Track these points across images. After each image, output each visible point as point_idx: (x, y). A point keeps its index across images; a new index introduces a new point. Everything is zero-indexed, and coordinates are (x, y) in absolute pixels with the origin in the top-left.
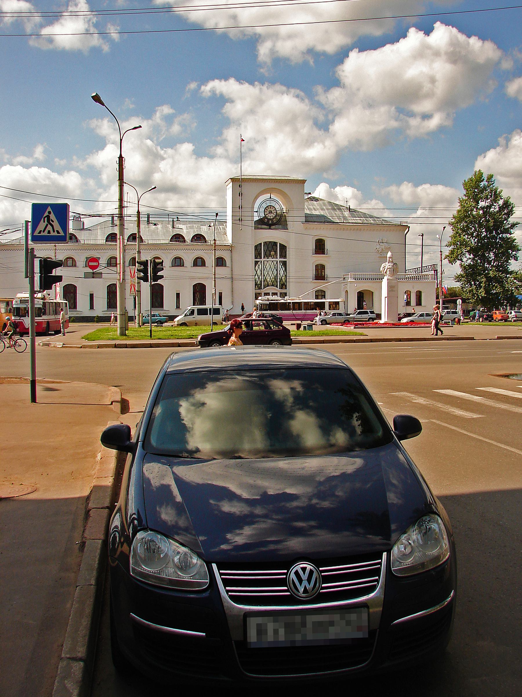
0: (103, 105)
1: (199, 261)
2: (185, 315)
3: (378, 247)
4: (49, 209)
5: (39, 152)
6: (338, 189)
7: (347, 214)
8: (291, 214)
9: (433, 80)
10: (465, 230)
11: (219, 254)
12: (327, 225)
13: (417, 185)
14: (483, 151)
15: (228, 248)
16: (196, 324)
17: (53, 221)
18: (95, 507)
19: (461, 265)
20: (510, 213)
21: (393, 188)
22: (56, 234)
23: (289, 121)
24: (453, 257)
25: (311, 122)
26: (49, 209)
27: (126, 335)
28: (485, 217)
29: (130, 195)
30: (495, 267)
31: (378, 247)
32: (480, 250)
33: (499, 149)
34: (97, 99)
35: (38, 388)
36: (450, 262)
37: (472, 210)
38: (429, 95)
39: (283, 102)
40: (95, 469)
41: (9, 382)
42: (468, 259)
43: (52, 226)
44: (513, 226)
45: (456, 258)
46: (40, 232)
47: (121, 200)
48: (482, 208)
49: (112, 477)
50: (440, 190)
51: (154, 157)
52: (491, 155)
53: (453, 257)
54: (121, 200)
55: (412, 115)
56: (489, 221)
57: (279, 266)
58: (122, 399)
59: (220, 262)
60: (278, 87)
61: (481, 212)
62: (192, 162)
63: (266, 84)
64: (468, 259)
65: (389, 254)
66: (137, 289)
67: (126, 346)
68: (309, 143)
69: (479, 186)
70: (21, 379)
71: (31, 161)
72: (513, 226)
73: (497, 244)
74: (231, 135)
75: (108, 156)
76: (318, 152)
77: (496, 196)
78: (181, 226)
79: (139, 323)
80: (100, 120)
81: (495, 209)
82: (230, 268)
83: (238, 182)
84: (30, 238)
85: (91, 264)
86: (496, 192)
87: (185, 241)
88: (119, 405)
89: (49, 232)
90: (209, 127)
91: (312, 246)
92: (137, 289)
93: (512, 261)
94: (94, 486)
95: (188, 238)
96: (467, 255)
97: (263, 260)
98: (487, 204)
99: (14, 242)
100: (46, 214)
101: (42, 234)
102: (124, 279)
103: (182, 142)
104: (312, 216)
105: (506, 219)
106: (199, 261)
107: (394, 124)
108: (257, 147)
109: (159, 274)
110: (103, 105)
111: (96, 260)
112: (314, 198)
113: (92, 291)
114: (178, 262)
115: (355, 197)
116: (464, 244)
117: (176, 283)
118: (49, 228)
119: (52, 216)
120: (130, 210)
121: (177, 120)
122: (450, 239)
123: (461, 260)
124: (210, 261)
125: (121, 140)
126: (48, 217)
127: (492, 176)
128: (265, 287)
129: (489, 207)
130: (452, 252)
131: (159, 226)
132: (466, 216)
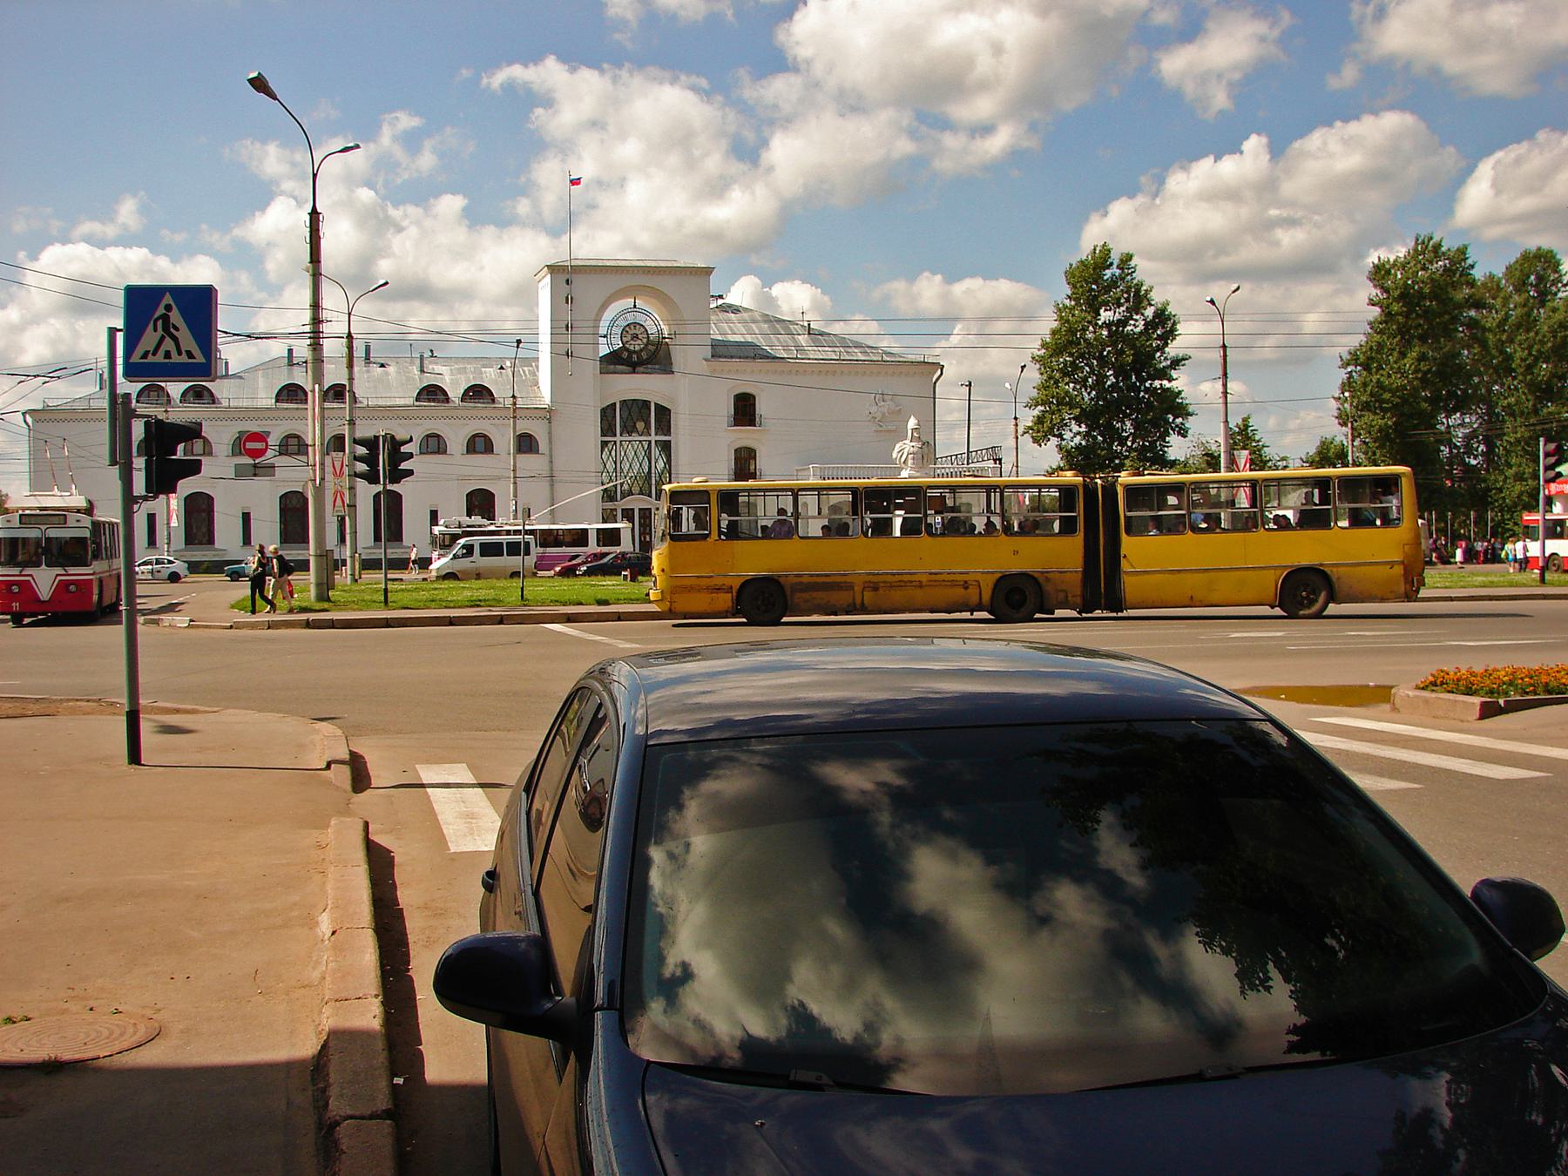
0: (275, 98)
1: (480, 443)
2: (455, 557)
3: (874, 409)
4: (168, 299)
5: (128, 211)
6: (777, 290)
7: (803, 339)
8: (679, 340)
9: (998, 49)
10: (1068, 372)
11: (524, 426)
12: (760, 365)
13: (951, 278)
14: (1102, 207)
15: (542, 414)
16: (478, 576)
17: (177, 329)
18: (349, 1112)
19: (1060, 448)
20: (1170, 334)
21: (899, 286)
22: (184, 359)
23: (679, 140)
24: (1043, 430)
25: (724, 144)
26: (168, 299)
27: (328, 600)
28: (1114, 345)
29: (332, 299)
30: (1136, 450)
31: (874, 409)
32: (1102, 414)
33: (1140, 199)
34: (259, 84)
35: (145, 727)
36: (1035, 441)
37: (1084, 330)
38: (983, 86)
39: (666, 102)
40: (318, 963)
41: (73, 712)
42: (1074, 434)
43: (175, 339)
44: (1176, 363)
45: (1050, 432)
46: (145, 356)
47: (316, 306)
48: (1108, 325)
49: (376, 996)
50: (1006, 289)
51: (378, 224)
52: (1120, 210)
53: (1043, 430)
54: (316, 306)
55: (946, 125)
56: (1122, 352)
57: (655, 452)
58: (352, 753)
59: (526, 444)
60: (653, 71)
61: (1105, 333)
62: (461, 235)
63: (627, 65)
64: (1074, 434)
65: (912, 423)
66: (347, 501)
67: (332, 624)
68: (717, 189)
69: (1101, 277)
70: (102, 705)
71: (111, 231)
72: (1176, 363)
73: (1140, 400)
74: (549, 174)
75: (281, 221)
76: (738, 209)
77: (1139, 299)
78: (438, 369)
79: (353, 575)
80: (258, 145)
81: (1136, 326)
82: (547, 459)
83: (565, 275)
84: (120, 369)
85: (250, 445)
86: (1138, 291)
87: (447, 400)
88: (346, 771)
89: (168, 355)
90: (496, 164)
91: (728, 408)
92: (347, 501)
93: (1173, 439)
94: (334, 1034)
95: (455, 393)
96: (1075, 428)
97: (618, 438)
98: (1117, 316)
99: (76, 405)
100: (161, 311)
101: (151, 359)
102: (322, 479)
103: (438, 194)
104: (726, 344)
105: (1161, 349)
106: (480, 443)
107: (905, 147)
108: (605, 200)
109: (404, 466)
110: (275, 98)
111: (260, 437)
112: (730, 306)
113: (244, 503)
114: (434, 445)
115: (817, 306)
116: (1065, 402)
117: (432, 492)
118: (168, 344)
119: (176, 317)
120: (335, 326)
121: (428, 144)
122: (1034, 393)
123: (1060, 436)
124: (504, 441)
125: (315, 176)
126: (165, 318)
127: (1129, 257)
128: (623, 497)
129: (1123, 323)
130: (1040, 420)
131: (391, 369)
132: (1071, 343)
